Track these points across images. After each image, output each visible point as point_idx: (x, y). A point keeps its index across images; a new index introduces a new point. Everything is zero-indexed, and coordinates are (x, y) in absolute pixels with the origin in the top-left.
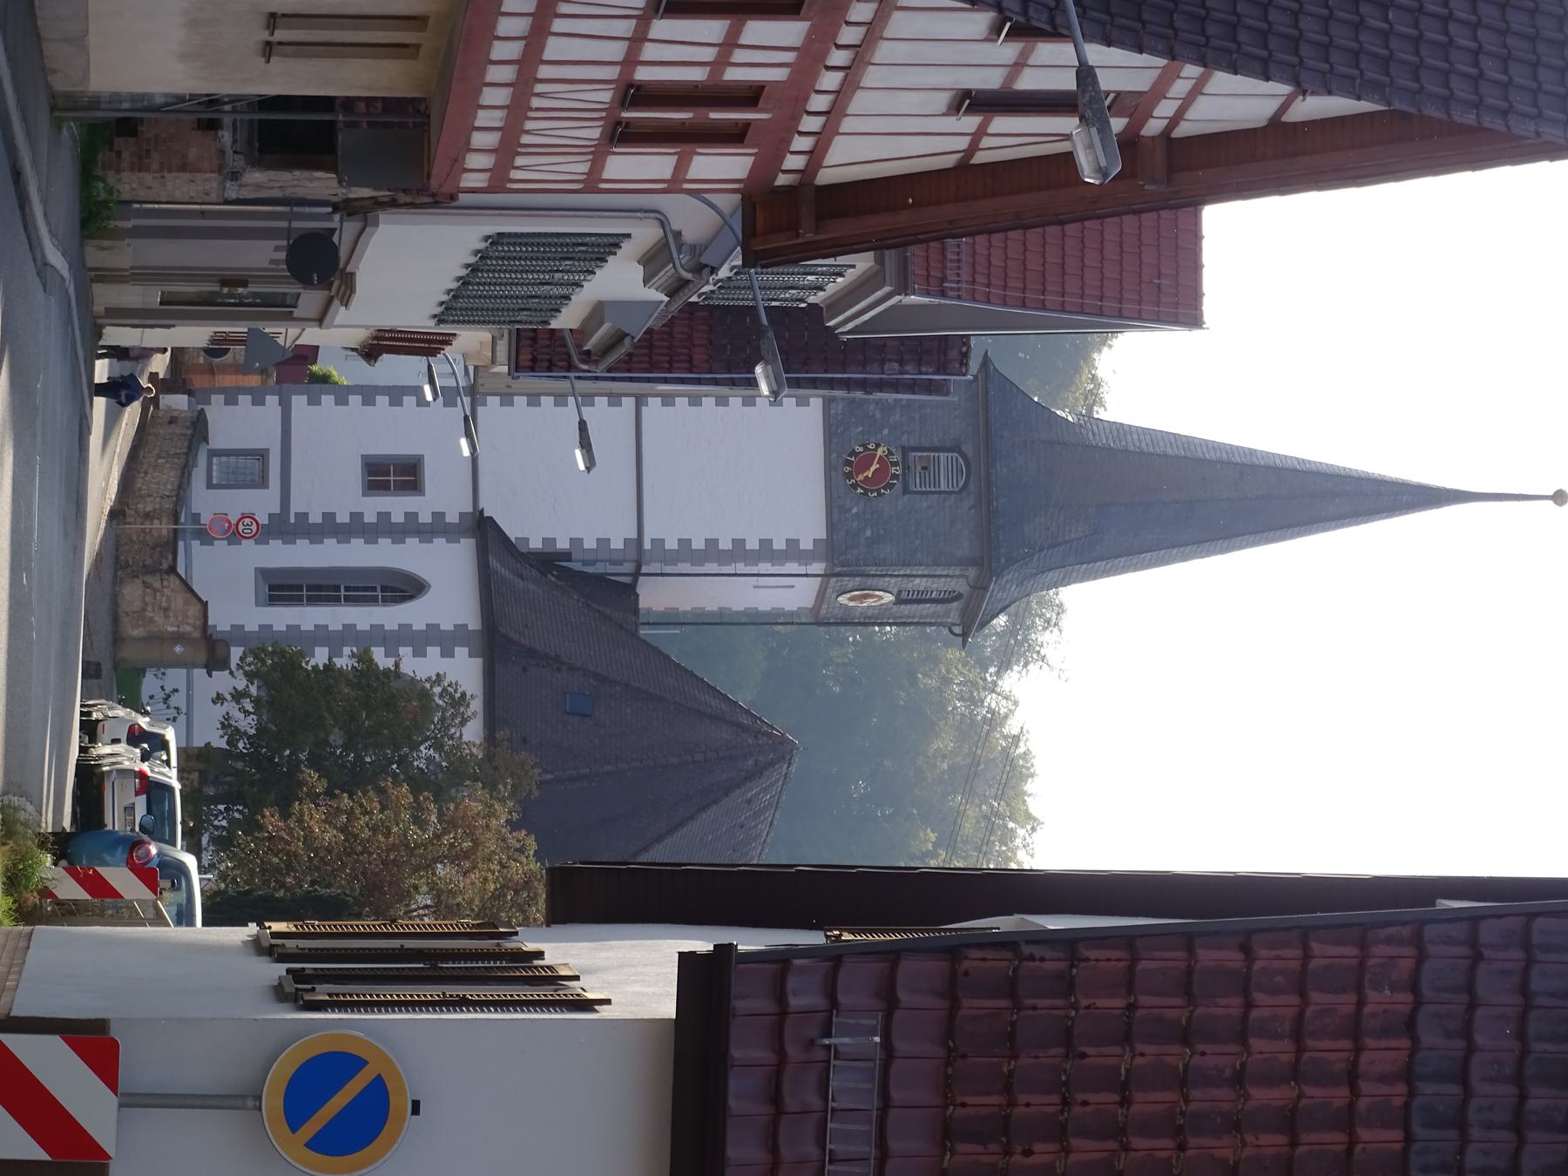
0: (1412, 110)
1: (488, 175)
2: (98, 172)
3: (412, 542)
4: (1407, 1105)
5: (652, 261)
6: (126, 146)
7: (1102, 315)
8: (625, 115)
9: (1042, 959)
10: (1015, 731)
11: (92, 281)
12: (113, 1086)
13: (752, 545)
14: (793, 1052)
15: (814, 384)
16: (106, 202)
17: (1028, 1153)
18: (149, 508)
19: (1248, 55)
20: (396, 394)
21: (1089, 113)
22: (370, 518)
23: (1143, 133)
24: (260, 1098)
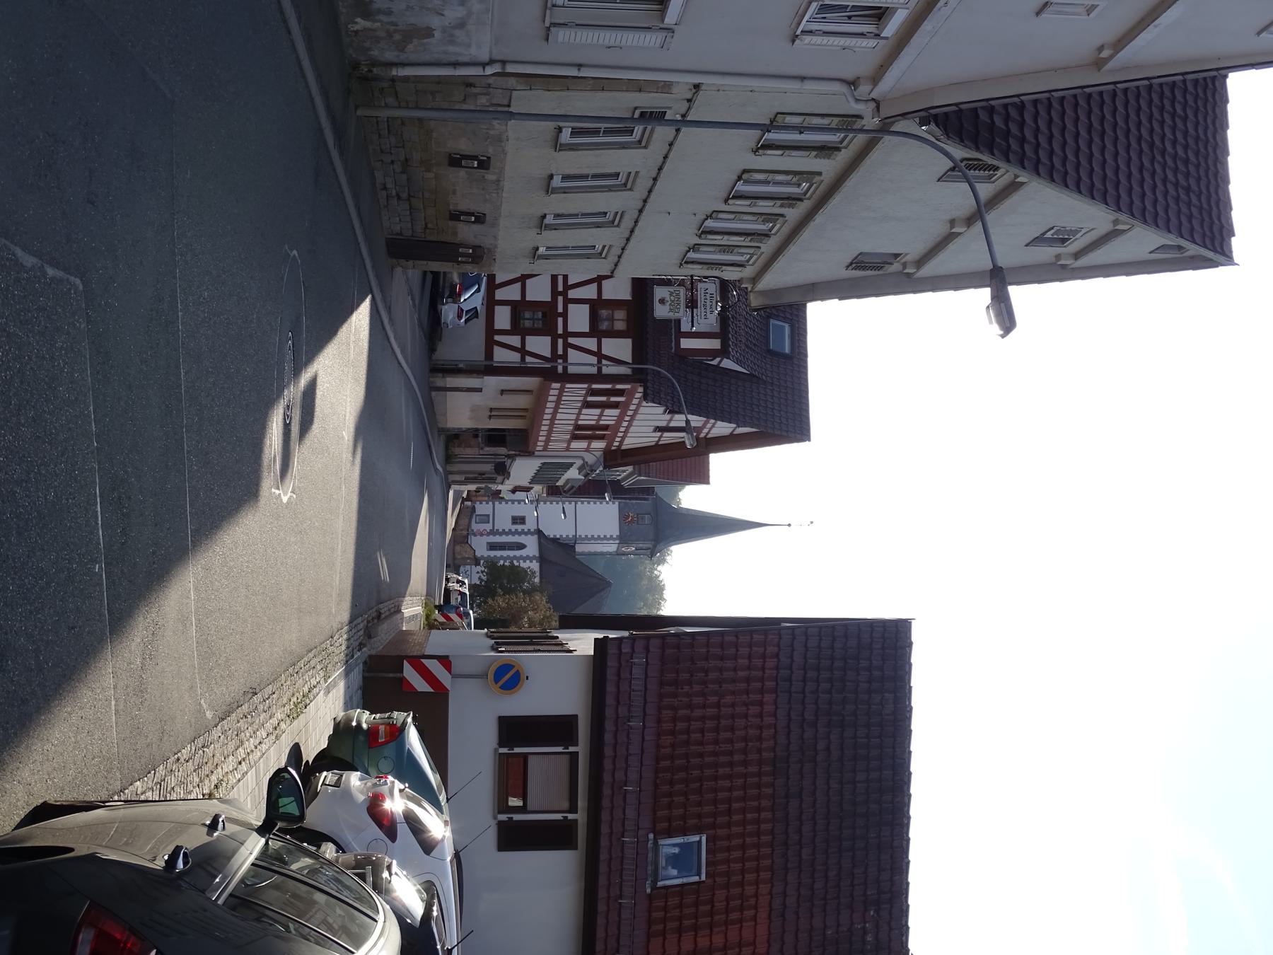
5: (580, 469)
14: (623, 663)
20: (519, 501)
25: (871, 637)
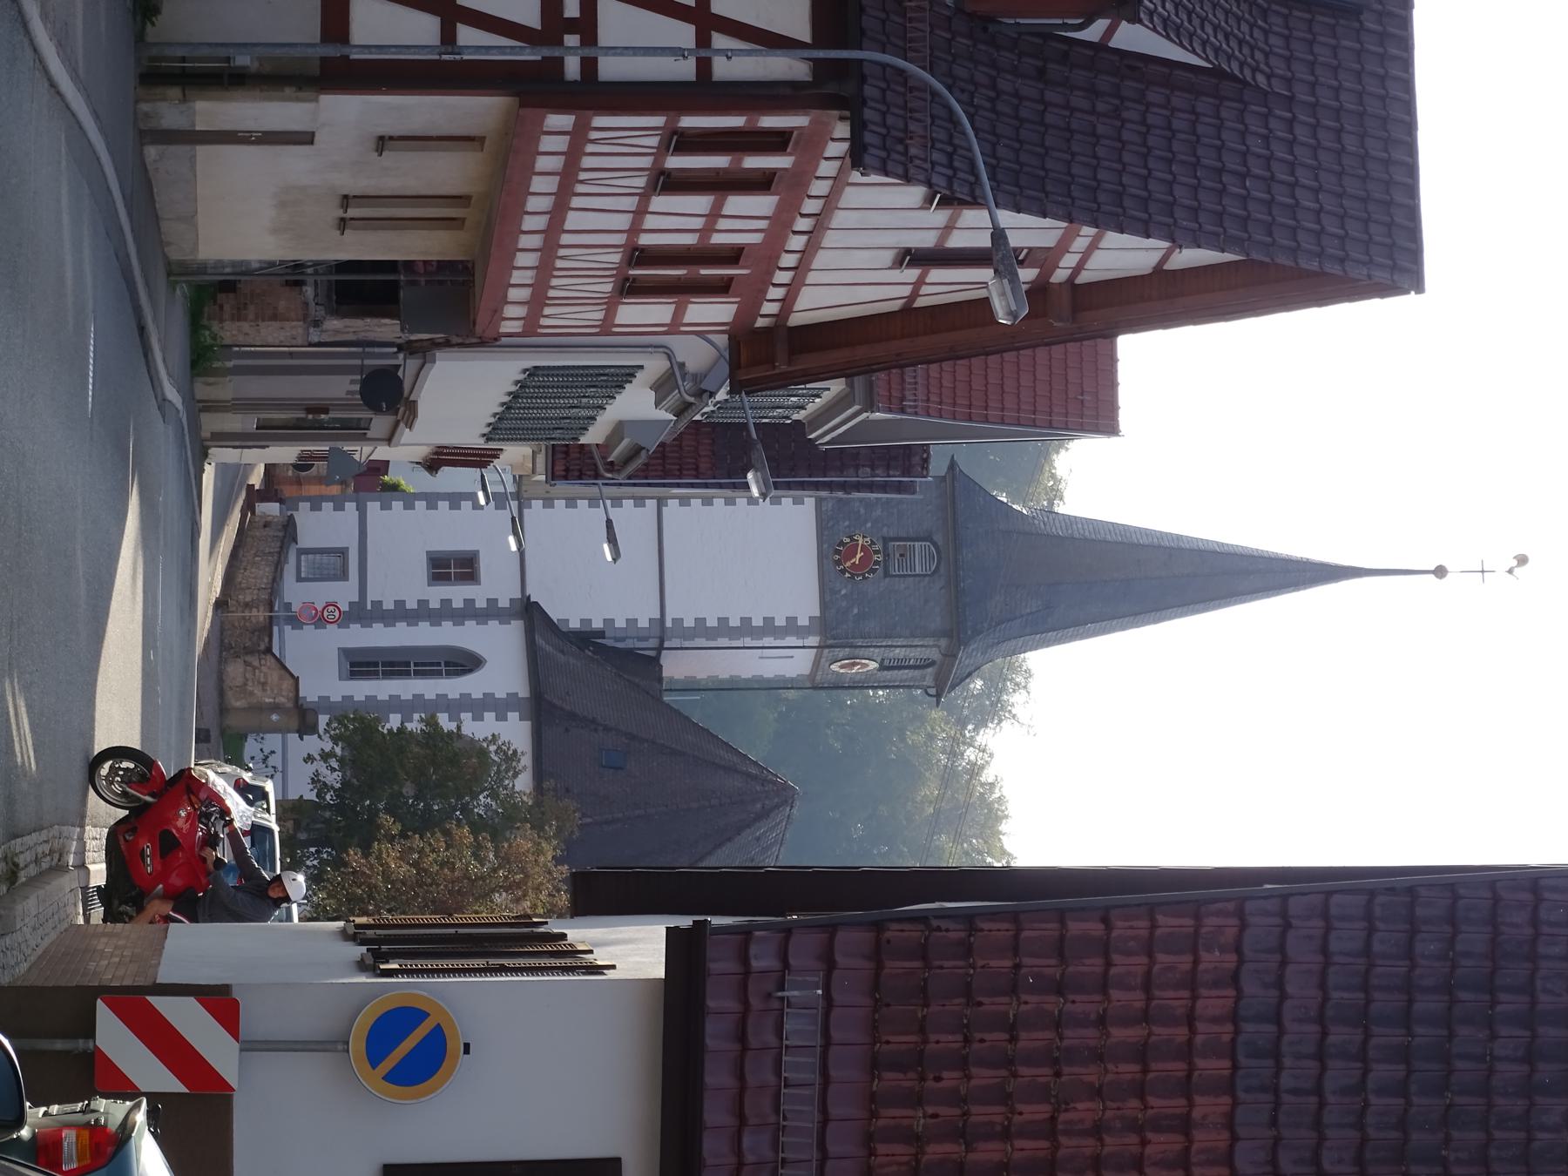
0: (1267, 260)
2: (205, 322)
3: (470, 624)
4: (1233, 1040)
5: (662, 387)
6: (229, 302)
7: (1051, 427)
9: (947, 930)
12: (235, 1034)
13: (734, 622)
14: (755, 1003)
15: (802, 486)
17: (938, 1079)
18: (248, 599)
19: (1133, 218)
20: (455, 500)
21: (1001, 268)
23: (1052, 280)
24: (347, 1043)
25: (1535, 921)
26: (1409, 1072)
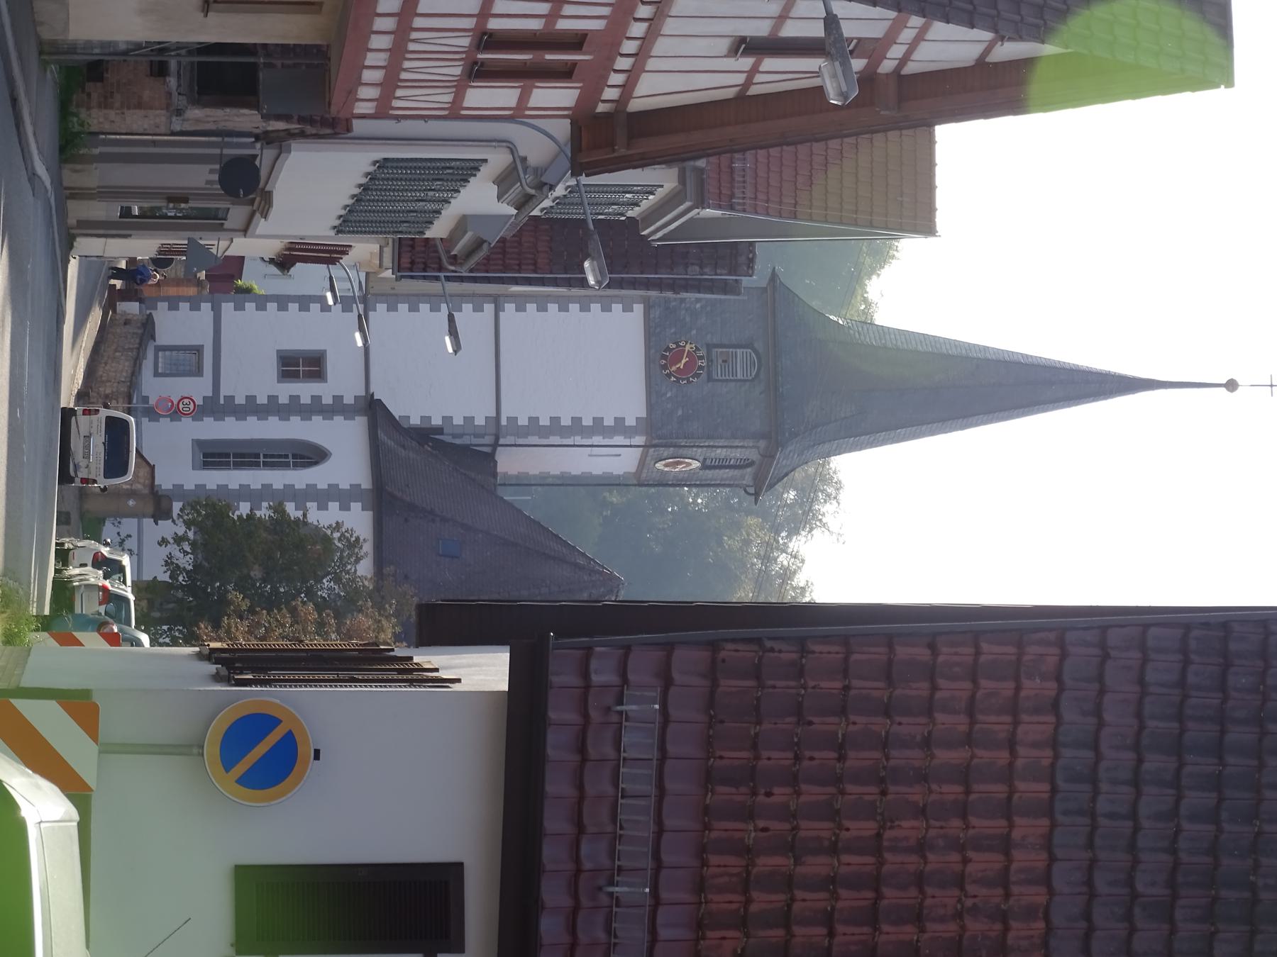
1: (375, 104)
3: (317, 419)
4: (1053, 765)
5: (504, 181)
6: (95, 90)
7: (872, 226)
8: (480, 56)
9: (780, 651)
10: (802, 584)
11: (67, 198)
14: (595, 715)
15: (634, 284)
16: (79, 133)
17: (769, 794)
18: (108, 391)
20: (304, 302)
21: (833, 51)
22: (284, 400)
26: (1220, 800)
